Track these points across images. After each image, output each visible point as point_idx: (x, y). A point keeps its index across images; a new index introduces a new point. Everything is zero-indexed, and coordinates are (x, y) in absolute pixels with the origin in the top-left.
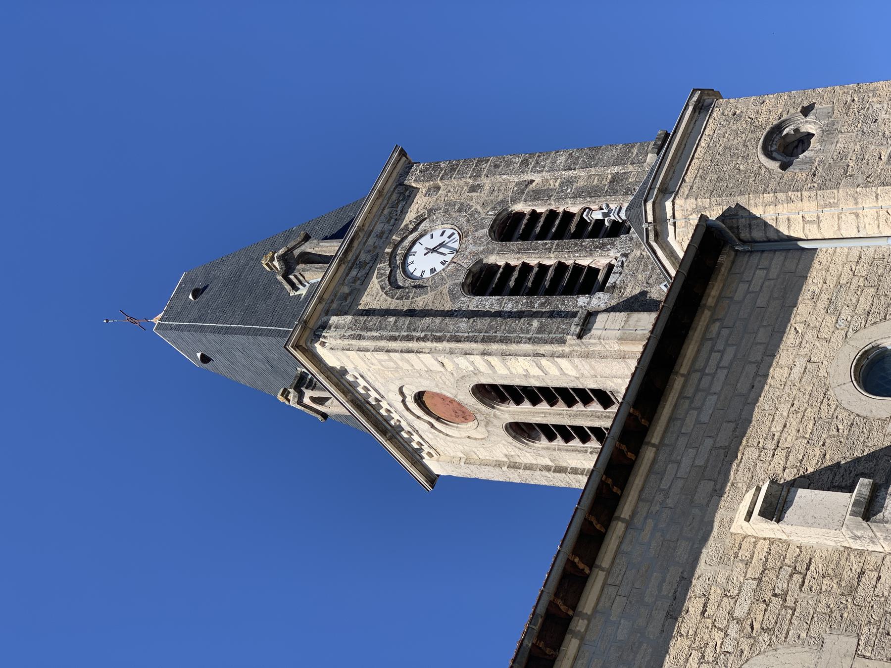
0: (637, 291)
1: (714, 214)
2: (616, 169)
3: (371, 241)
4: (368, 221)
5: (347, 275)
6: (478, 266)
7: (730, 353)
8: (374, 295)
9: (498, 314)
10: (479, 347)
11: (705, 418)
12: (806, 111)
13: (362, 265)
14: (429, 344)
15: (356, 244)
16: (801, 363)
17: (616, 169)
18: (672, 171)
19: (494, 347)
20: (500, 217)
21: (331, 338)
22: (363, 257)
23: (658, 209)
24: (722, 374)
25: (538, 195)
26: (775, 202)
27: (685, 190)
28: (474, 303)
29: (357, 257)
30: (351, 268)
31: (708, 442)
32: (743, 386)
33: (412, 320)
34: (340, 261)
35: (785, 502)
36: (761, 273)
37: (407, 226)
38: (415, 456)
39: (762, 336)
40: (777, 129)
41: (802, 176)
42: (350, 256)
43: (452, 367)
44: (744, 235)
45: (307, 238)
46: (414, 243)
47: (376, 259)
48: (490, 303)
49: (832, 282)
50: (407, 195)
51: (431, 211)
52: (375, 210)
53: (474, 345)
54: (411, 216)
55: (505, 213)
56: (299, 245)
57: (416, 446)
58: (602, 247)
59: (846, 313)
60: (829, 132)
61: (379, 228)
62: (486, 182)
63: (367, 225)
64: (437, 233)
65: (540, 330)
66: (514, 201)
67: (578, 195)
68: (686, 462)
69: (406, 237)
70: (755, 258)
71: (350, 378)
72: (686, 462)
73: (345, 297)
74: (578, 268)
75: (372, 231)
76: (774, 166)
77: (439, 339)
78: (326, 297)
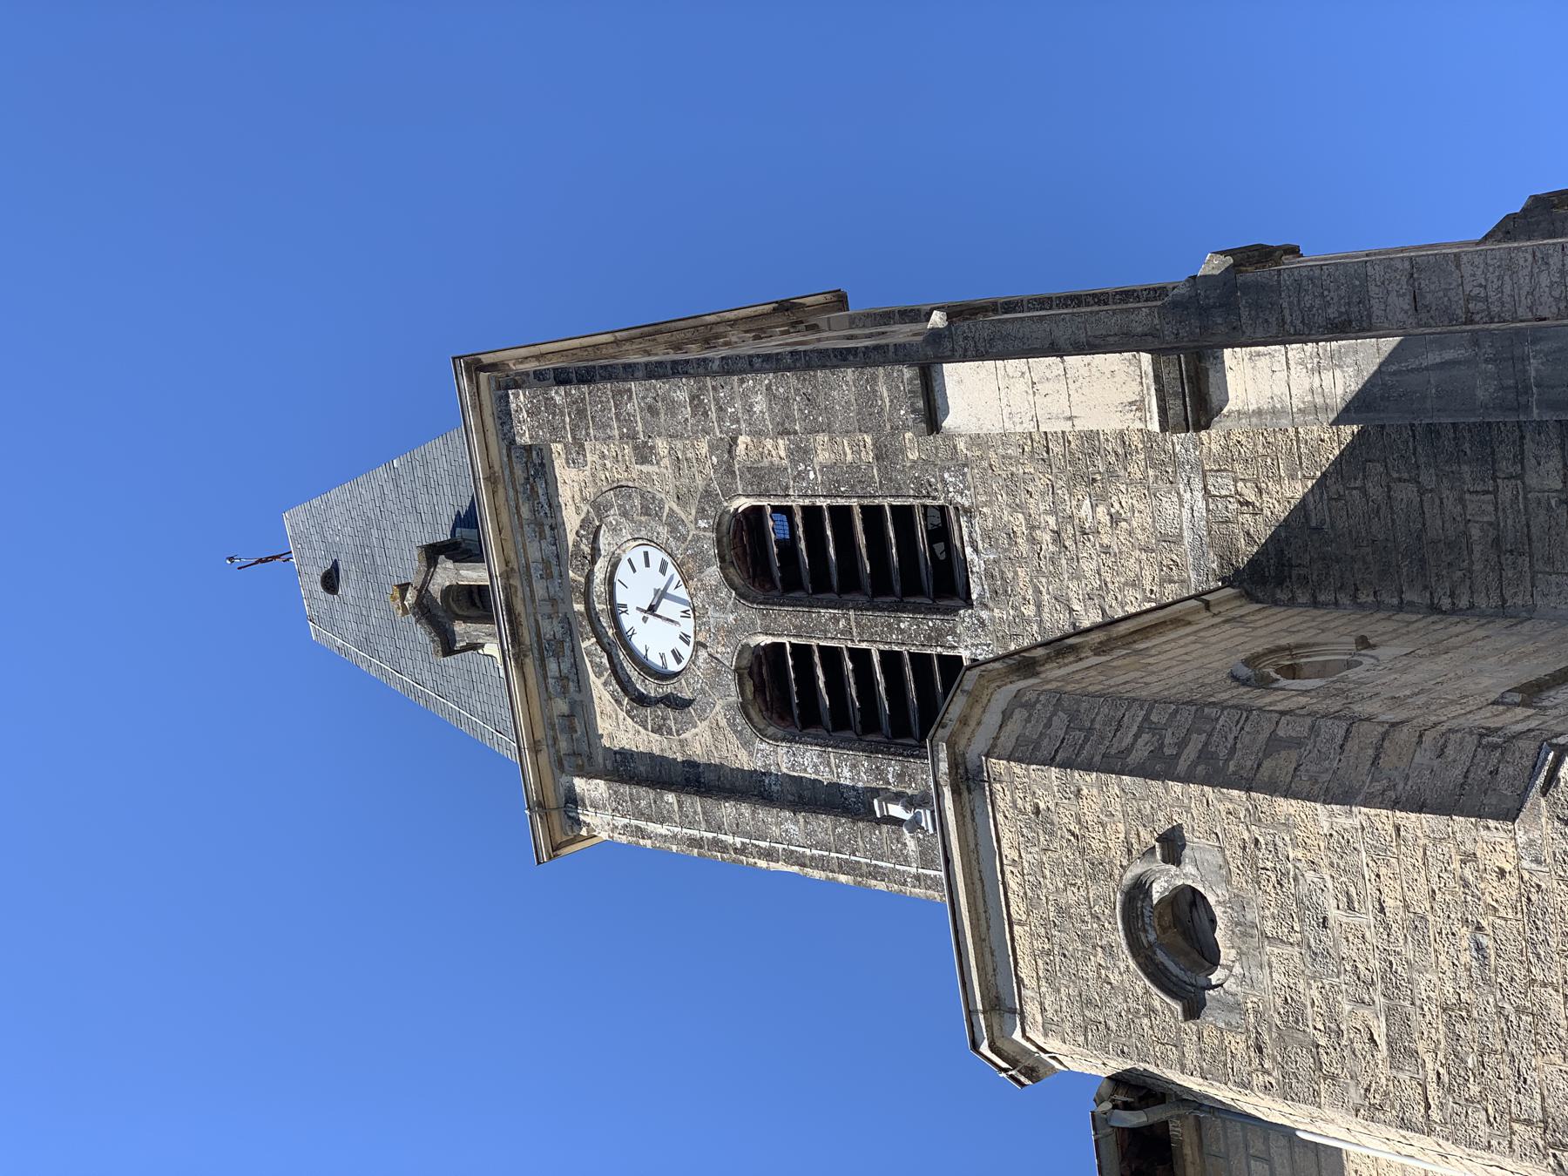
4: (509, 545)
5: (545, 677)
6: (747, 655)
15: (519, 607)
18: (988, 956)
20: (724, 528)
29: (538, 635)
30: (542, 660)
34: (516, 661)
37: (576, 545)
42: (527, 636)
46: (610, 582)
52: (504, 517)
54: (572, 520)
55: (727, 517)
63: (513, 556)
69: (591, 572)
75: (528, 567)
78: (539, 735)
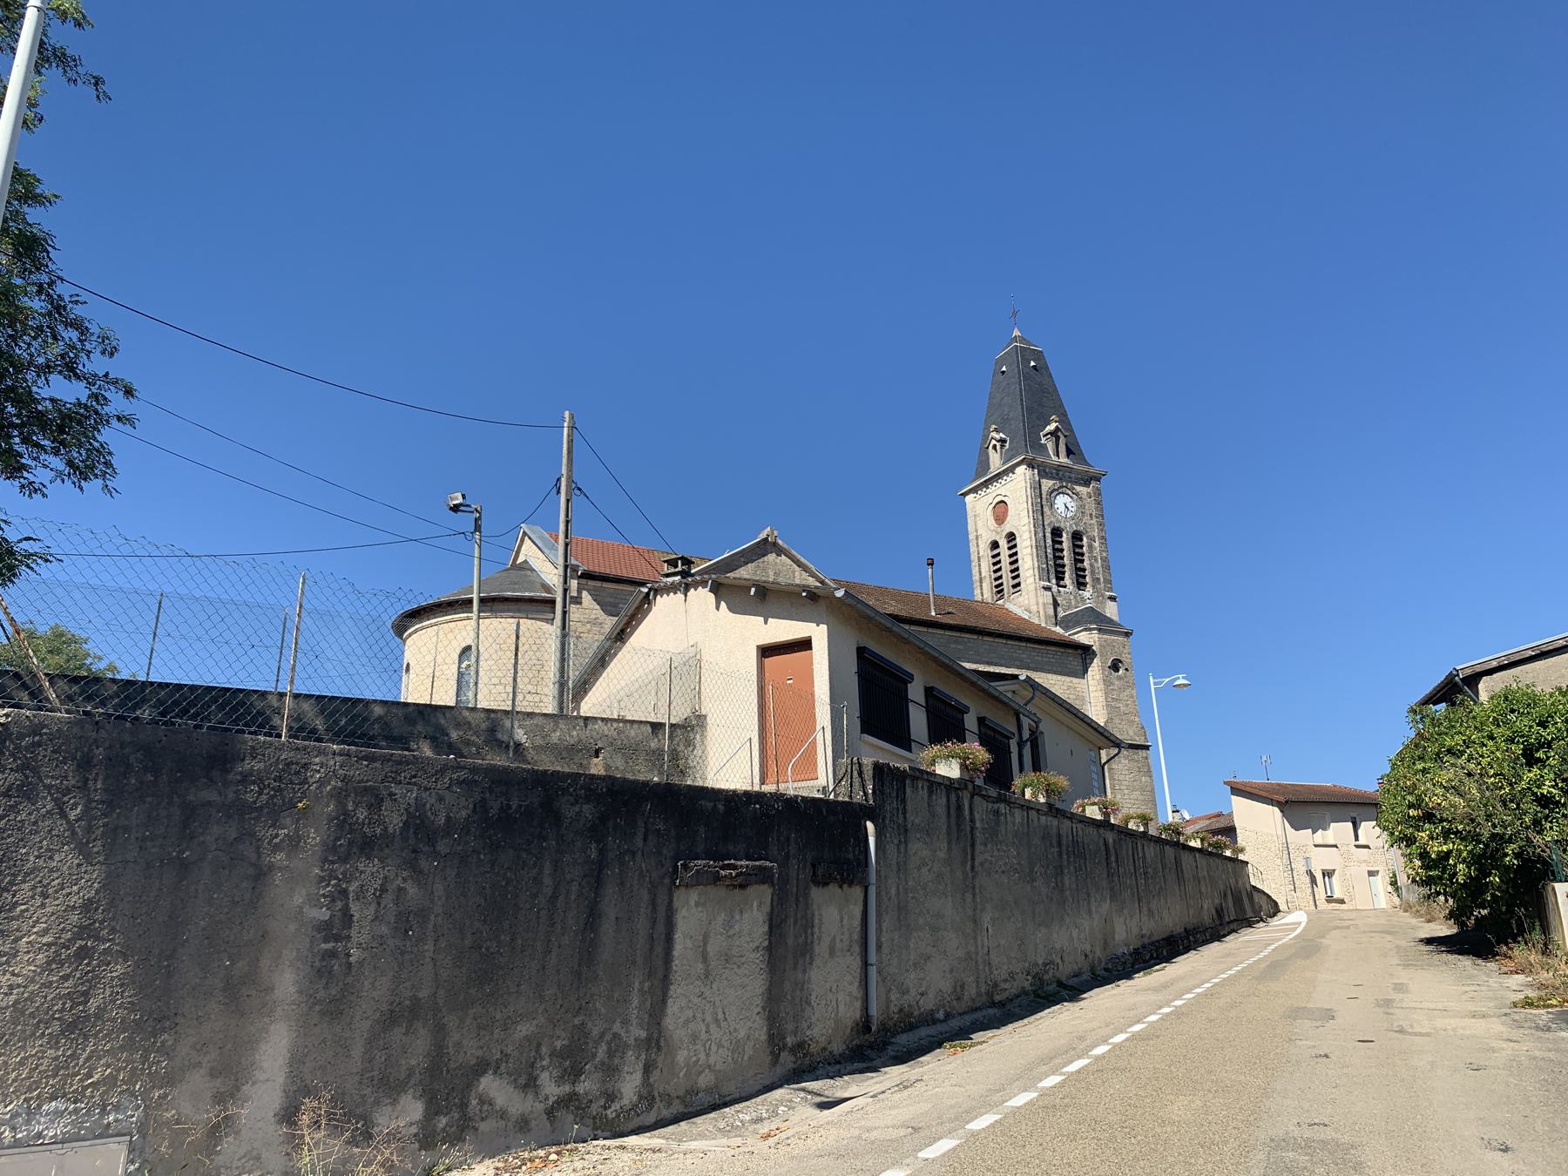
8: (1047, 484)
21: (1029, 472)
25: (1090, 546)
28: (1048, 530)
33: (1041, 504)
35: (639, 608)
43: (1021, 521)
47: (1060, 479)
48: (1048, 535)
54: (1078, 488)
60: (1120, 678)
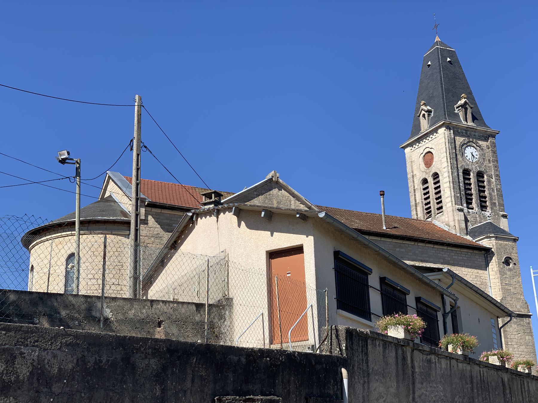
0: (469, 219)
1: (493, 250)
2: (497, 204)
3: (473, 133)
7: (466, 258)
8: (460, 140)
9: (459, 182)
10: (451, 181)
11: (454, 257)
12: (515, 264)
13: (466, 133)
14: (450, 165)
16: (466, 273)
17: (497, 204)
19: (452, 184)
21: (447, 132)
22: (468, 132)
23: (492, 237)
24: (461, 258)
25: (489, 182)
26: (496, 262)
27: (497, 242)
28: (461, 171)
31: (449, 259)
32: (460, 263)
33: (455, 153)
36: (481, 260)
38: (411, 145)
39: (470, 264)
40: (511, 259)
41: (501, 266)
43: (442, 164)
44: (488, 256)
45: (471, 108)
46: (473, 147)
47: (468, 137)
49: (481, 275)
50: (486, 140)
51: (482, 149)
53: (451, 179)
54: (480, 143)
56: (470, 106)
57: (414, 146)
58: (478, 206)
59: (476, 279)
60: (510, 270)
61: (477, 134)
62: (491, 164)
64: (477, 153)
65: (457, 197)
66: (487, 176)
67: (490, 194)
68: (445, 256)
70: (484, 258)
71: (435, 134)
72: (445, 256)
73: (458, 131)
74: (472, 199)
76: (503, 260)
77: (451, 168)
